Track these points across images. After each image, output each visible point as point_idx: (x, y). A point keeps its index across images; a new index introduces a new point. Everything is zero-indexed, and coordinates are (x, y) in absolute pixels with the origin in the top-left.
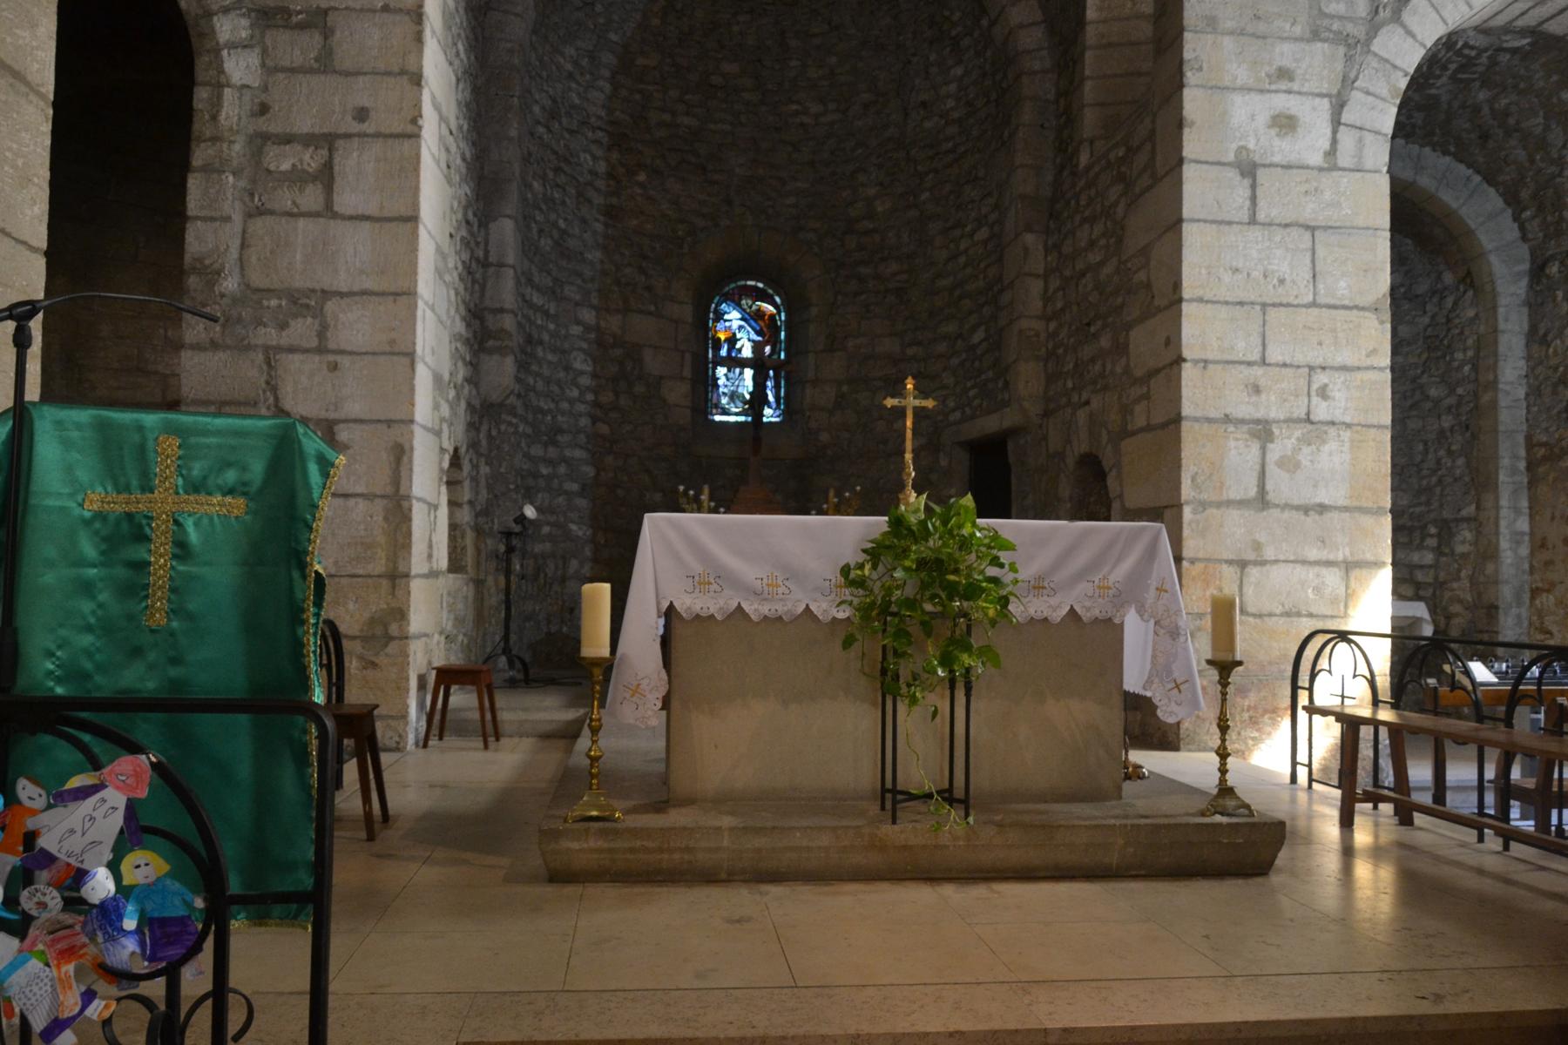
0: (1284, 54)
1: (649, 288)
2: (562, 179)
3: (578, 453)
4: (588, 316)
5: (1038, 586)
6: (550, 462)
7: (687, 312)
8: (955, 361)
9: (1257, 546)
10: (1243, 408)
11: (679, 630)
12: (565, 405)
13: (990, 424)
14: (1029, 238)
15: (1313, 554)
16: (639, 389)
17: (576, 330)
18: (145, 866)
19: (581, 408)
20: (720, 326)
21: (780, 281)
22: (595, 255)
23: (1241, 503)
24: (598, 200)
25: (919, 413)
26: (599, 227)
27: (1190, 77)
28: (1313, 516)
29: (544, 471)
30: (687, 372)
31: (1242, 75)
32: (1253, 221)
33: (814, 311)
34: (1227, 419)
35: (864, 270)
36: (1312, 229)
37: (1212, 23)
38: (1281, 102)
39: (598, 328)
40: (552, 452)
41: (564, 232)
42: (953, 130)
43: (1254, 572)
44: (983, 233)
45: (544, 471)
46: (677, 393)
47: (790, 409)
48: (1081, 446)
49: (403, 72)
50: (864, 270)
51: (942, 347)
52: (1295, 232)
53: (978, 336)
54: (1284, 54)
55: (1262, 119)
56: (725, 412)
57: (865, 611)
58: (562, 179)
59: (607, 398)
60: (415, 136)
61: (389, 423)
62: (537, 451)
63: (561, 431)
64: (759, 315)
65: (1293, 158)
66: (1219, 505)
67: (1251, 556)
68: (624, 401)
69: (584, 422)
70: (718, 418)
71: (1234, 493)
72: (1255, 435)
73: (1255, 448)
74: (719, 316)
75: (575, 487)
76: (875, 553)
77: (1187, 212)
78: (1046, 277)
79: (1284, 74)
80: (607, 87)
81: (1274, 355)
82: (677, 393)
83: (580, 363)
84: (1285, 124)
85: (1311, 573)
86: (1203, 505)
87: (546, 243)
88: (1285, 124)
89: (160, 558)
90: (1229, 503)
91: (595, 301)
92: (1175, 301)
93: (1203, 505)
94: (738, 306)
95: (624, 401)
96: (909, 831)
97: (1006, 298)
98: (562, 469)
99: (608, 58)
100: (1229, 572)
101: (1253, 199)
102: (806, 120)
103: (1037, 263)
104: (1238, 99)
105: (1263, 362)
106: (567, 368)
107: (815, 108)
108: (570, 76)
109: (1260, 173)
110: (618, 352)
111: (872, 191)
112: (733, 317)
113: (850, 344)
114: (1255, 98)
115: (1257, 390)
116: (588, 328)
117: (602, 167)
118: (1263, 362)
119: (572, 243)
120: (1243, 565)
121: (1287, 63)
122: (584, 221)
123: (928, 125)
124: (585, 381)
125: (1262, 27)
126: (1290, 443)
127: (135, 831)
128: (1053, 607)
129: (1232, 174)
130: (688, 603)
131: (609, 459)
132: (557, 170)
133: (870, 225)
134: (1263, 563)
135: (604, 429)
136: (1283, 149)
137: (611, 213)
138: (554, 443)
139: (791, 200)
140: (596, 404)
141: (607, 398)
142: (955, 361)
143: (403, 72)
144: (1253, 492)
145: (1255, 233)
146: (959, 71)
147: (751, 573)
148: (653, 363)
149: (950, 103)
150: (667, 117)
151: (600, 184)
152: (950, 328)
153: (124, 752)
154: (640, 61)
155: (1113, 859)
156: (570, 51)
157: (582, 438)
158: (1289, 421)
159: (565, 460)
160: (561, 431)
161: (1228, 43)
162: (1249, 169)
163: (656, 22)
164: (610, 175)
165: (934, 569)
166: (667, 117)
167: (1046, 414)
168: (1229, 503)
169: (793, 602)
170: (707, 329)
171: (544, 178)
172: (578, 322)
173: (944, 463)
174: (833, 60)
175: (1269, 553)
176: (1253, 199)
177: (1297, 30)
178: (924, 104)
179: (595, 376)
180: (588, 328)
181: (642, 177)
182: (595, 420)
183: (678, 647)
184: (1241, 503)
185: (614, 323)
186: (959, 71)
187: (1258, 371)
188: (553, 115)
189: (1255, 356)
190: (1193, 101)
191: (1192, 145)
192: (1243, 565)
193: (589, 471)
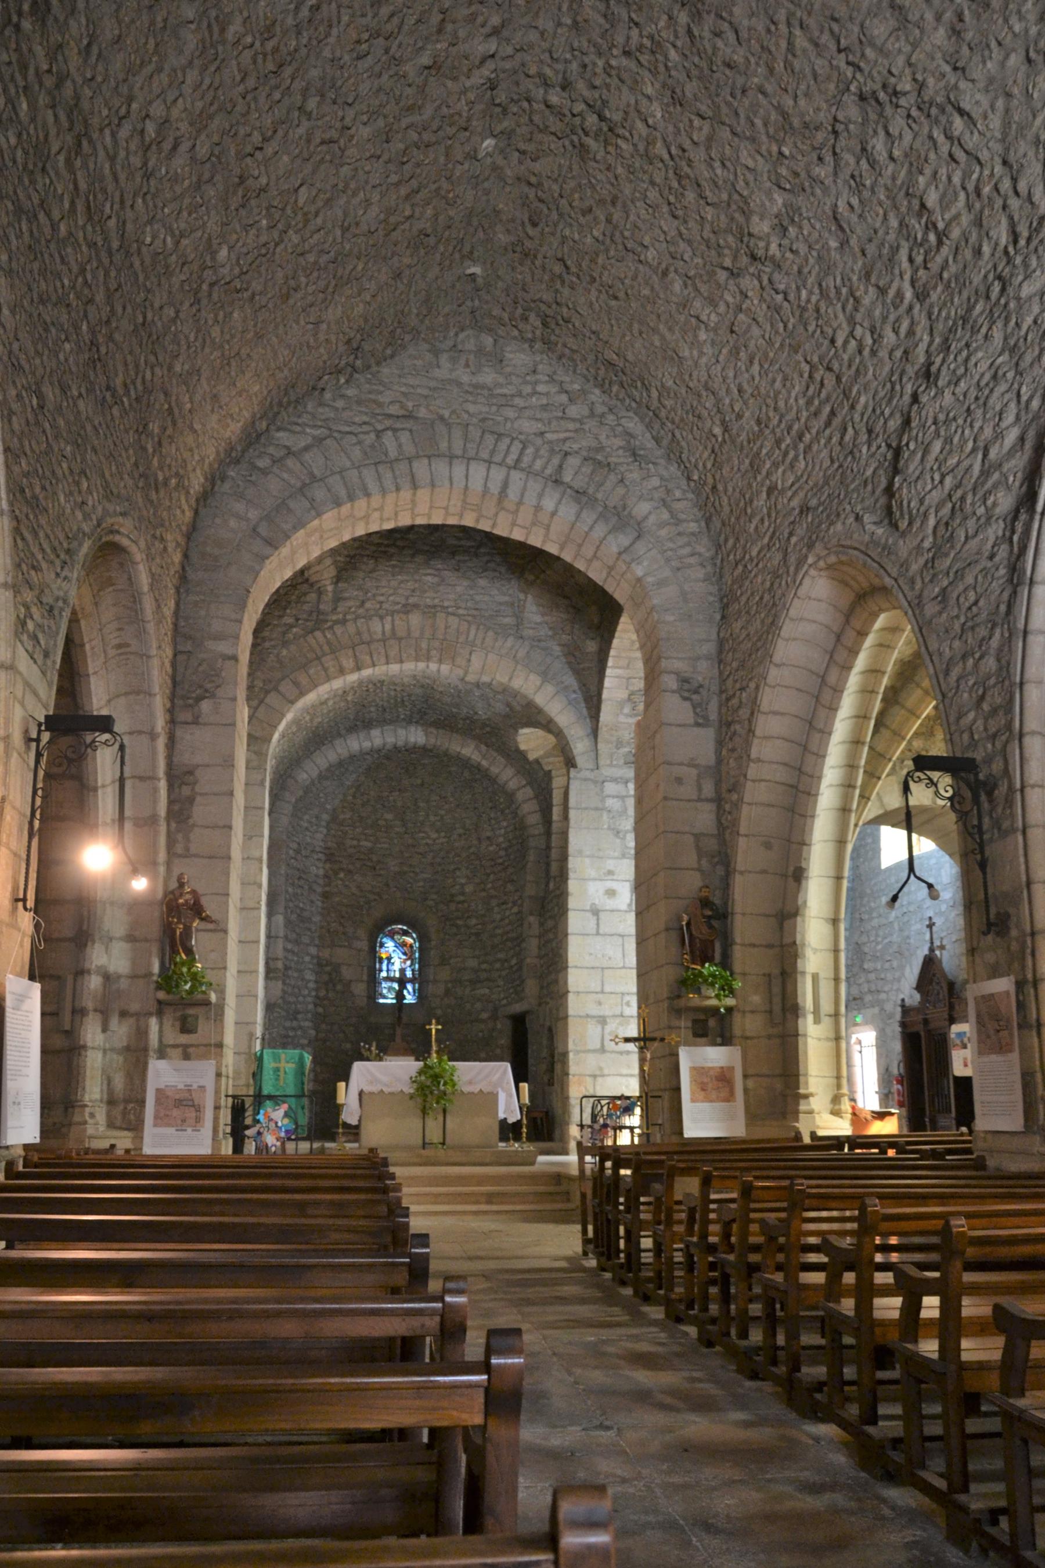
0: (610, 864)
1: (344, 933)
2: (301, 883)
3: (307, 1024)
4: (313, 950)
5: (470, 1083)
6: (293, 1029)
7: (363, 945)
8: (504, 973)
9: (601, 1069)
10: (594, 1010)
11: (364, 1097)
12: (301, 999)
13: (518, 1008)
14: (532, 919)
15: (625, 1071)
16: (339, 987)
17: (307, 959)
18: (286, 1121)
19: (309, 999)
20: (383, 950)
21: (415, 925)
22: (317, 919)
23: (595, 1051)
24: (319, 890)
25: (437, 1030)
26: (319, 904)
27: (571, 875)
28: (625, 1056)
29: (291, 1034)
30: (365, 978)
31: (593, 873)
32: (598, 934)
33: (433, 943)
34: (588, 1016)
35: (460, 922)
36: (622, 936)
37: (580, 852)
38: (609, 884)
39: (318, 957)
40: (295, 1024)
41: (302, 909)
42: (502, 853)
43: (600, 1080)
44: (515, 910)
45: (291, 1034)
46: (360, 989)
47: (421, 995)
48: (548, 1024)
49: (255, 883)
50: (460, 922)
51: (498, 965)
52: (615, 938)
53: (514, 961)
54: (610, 864)
55: (601, 891)
56: (385, 997)
57: (417, 1090)
58: (301, 883)
59: (323, 993)
60: (259, 909)
61: (247, 1023)
62: (288, 1024)
63: (299, 1013)
64: (404, 944)
65: (614, 907)
66: (584, 1052)
67: (598, 1073)
68: (331, 995)
69: (311, 1007)
70: (381, 1001)
71: (591, 1047)
72: (599, 1022)
73: (599, 1028)
74: (382, 945)
75: (306, 1042)
76: (420, 1072)
77: (570, 931)
78: (540, 937)
79: (610, 873)
80: (325, 831)
81: (607, 989)
82: (360, 989)
83: (309, 976)
84: (611, 893)
85: (624, 1080)
86: (577, 1052)
87: (294, 917)
88: (611, 893)
89: (282, 1074)
90: (589, 1051)
91: (317, 942)
92: (566, 968)
93: (577, 1052)
94: (393, 939)
95: (331, 995)
96: (428, 1152)
97: (524, 945)
98: (299, 1033)
99: (325, 817)
100: (589, 1080)
101: (598, 924)
102: (430, 842)
103: (536, 930)
104: (591, 883)
105: (602, 992)
106: (303, 979)
107: (434, 835)
108: (307, 829)
109: (602, 915)
110: (328, 969)
111: (463, 881)
112: (390, 945)
113: (452, 961)
114: (598, 883)
115: (600, 1003)
116: (313, 957)
117: (321, 872)
118: (602, 992)
119: (306, 914)
120: (595, 1076)
121: (611, 868)
122: (312, 902)
123: (491, 848)
124: (312, 985)
125: (601, 854)
126: (614, 1025)
127: (286, 1115)
128: (475, 1089)
129: (589, 915)
130: (367, 1088)
131: (324, 1026)
132: (300, 878)
133: (462, 898)
134: (603, 1076)
135: (320, 1010)
136: (610, 903)
137: (326, 896)
138: (296, 1019)
139: (421, 884)
140: (317, 997)
141: (323, 993)
142: (504, 973)
143: (255, 883)
144: (598, 1046)
145: (599, 938)
146: (505, 824)
147: (384, 1079)
148: (347, 973)
149: (501, 839)
150: (355, 843)
151: (321, 881)
152: (501, 956)
153: (956, 847)
154: (342, 817)
155: (488, 1160)
156: (306, 817)
157: (309, 1015)
158: (615, 1016)
159: (301, 1028)
160: (299, 1013)
161: (587, 861)
162: (596, 912)
163: (350, 798)
164: (326, 876)
165: (436, 1078)
166: (355, 843)
167: (540, 1005)
168: (589, 1051)
169: (397, 1088)
170: (375, 952)
171: (293, 884)
172: (308, 954)
173: (499, 1026)
174: (443, 812)
175: (606, 1072)
176: (598, 924)
177: (616, 854)
178: (488, 838)
179: (316, 982)
180: (313, 957)
181: (342, 875)
182: (316, 1005)
183: (364, 1102)
184: (595, 1051)
185: (326, 953)
186: (505, 824)
187: (600, 996)
188: (298, 852)
189: (599, 989)
190: (572, 885)
191: (572, 903)
192: (595, 1076)
193: (313, 1032)
